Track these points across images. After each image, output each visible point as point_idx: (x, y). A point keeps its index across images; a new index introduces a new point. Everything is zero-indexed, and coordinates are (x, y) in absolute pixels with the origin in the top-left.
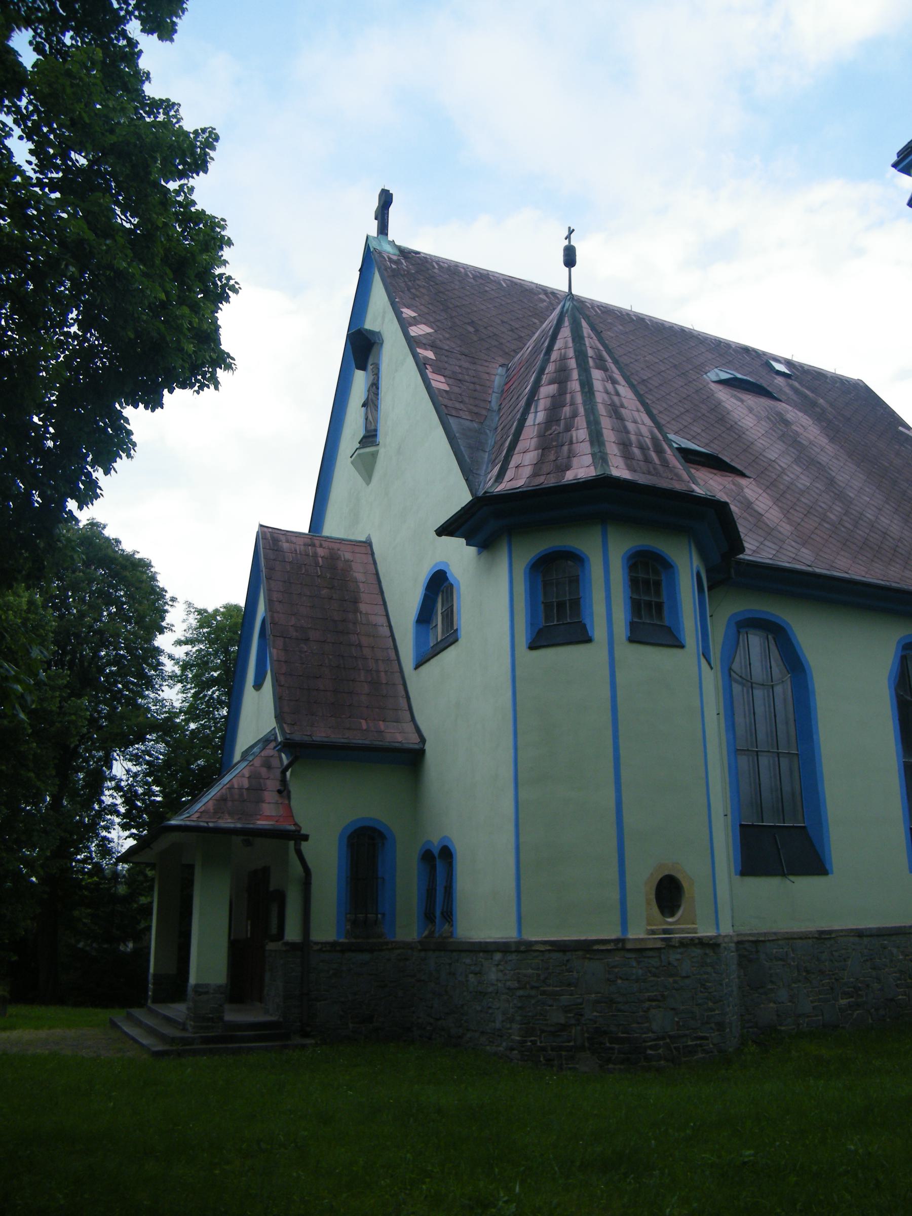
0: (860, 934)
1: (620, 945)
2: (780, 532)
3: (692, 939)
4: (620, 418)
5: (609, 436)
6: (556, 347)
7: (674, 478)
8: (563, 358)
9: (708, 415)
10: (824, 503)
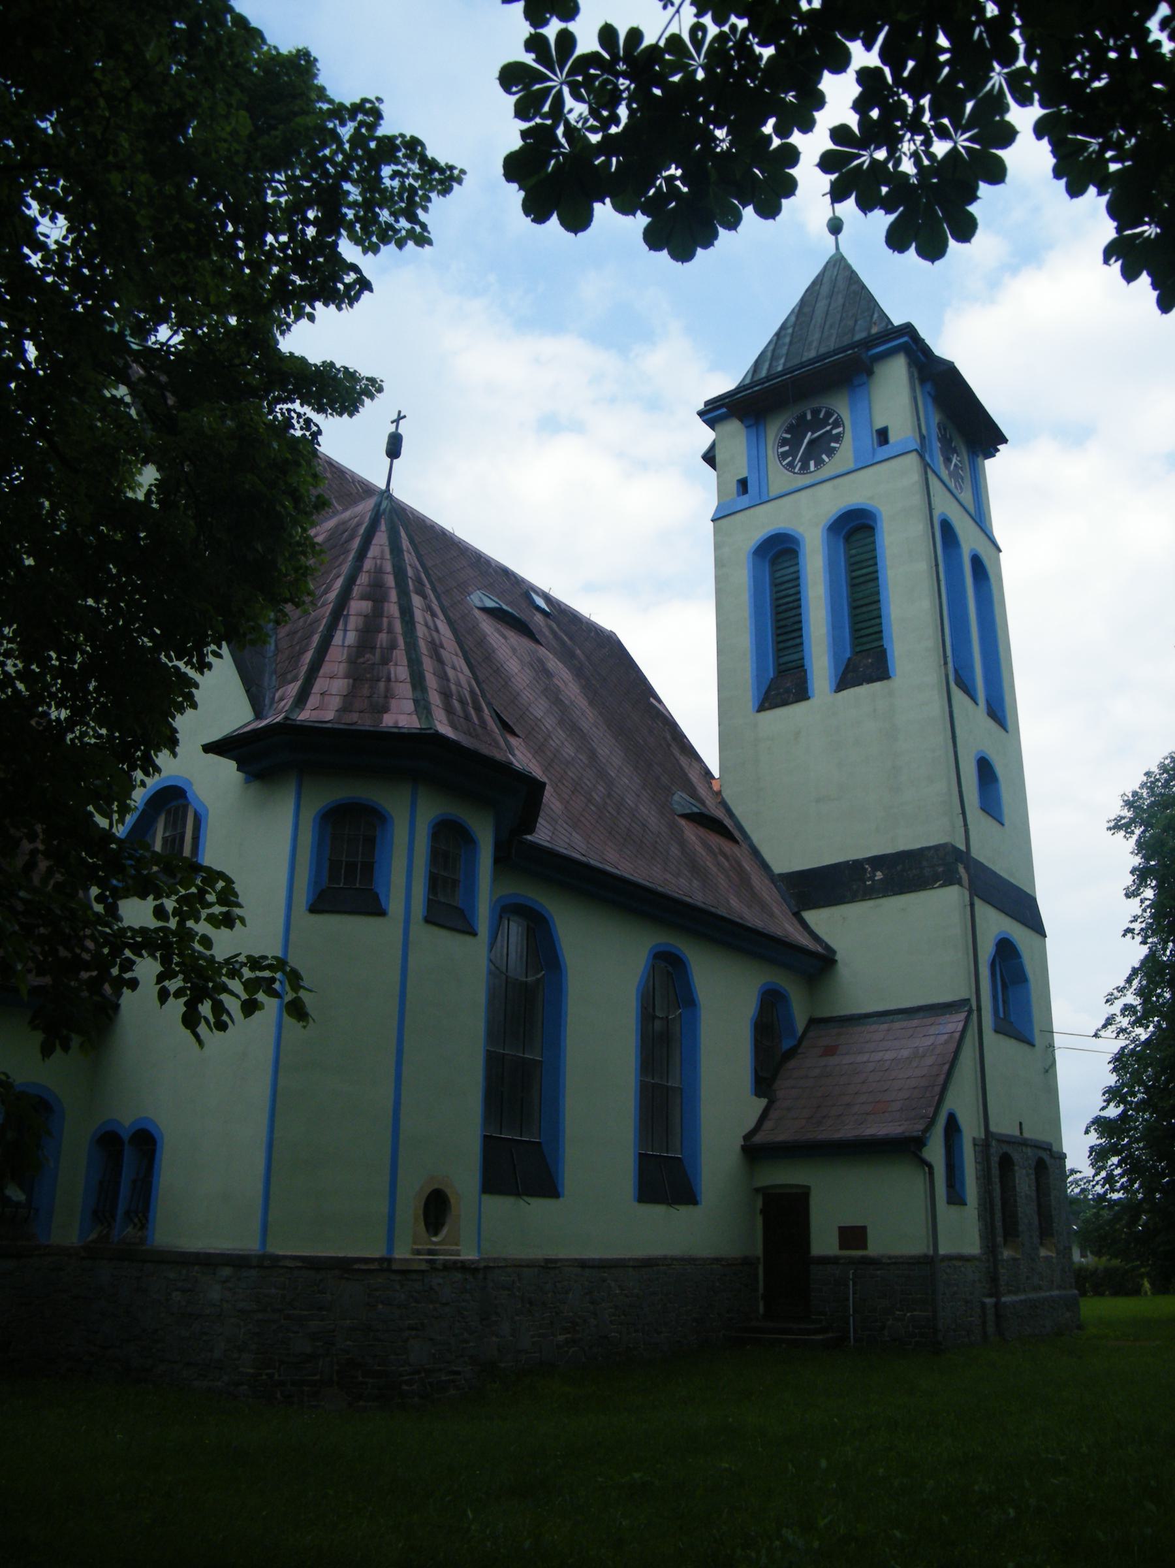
0: (583, 1264)
1: (385, 1265)
2: (552, 810)
3: (455, 1262)
4: (440, 660)
5: (431, 681)
6: (370, 554)
7: (493, 744)
8: (379, 571)
9: (475, 649)
10: (589, 780)
